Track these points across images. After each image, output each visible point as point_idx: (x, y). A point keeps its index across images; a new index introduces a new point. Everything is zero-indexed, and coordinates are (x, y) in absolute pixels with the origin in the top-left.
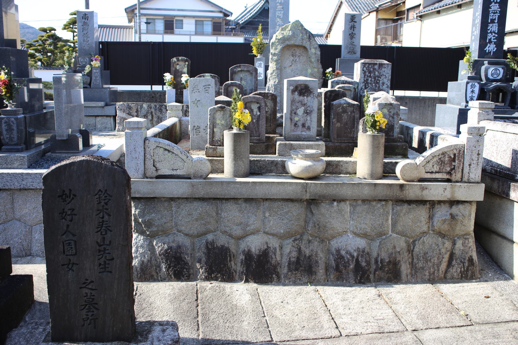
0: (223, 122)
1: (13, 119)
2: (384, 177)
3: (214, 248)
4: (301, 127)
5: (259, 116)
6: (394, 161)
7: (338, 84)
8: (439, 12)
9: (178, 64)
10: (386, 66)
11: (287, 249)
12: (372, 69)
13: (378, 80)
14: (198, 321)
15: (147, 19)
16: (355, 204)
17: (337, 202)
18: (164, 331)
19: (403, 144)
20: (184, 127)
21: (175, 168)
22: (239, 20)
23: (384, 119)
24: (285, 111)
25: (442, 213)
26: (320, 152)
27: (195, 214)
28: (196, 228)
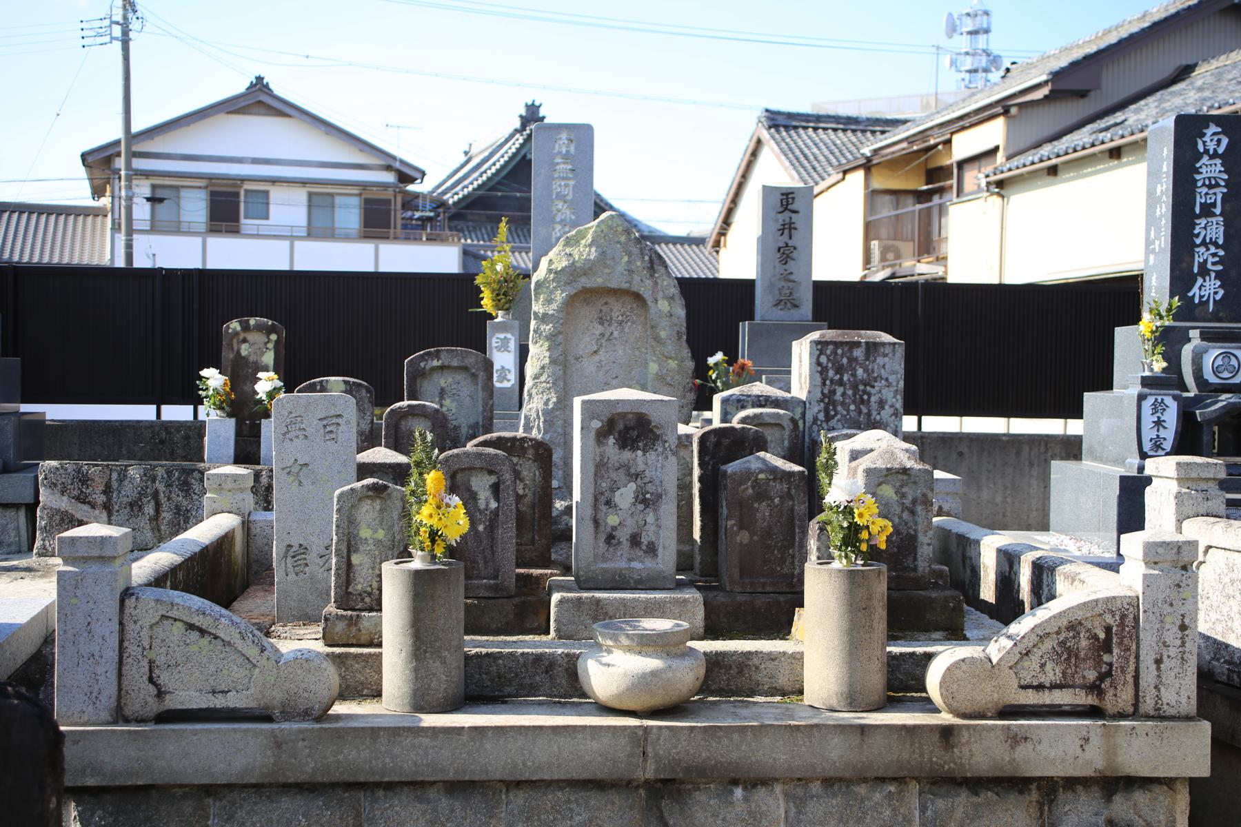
0: (381, 534)
2: (889, 703)
4: (626, 545)
5: (496, 513)
6: (920, 650)
7: (743, 407)
8: (1053, 171)
9: (245, 341)
10: (888, 350)
12: (845, 361)
13: (865, 392)
15: (154, 187)
16: (800, 792)
17: (745, 789)
19: (948, 593)
20: (259, 541)
21: (223, 687)
22: (444, 193)
23: (882, 522)
24: (577, 496)
26: (686, 625)
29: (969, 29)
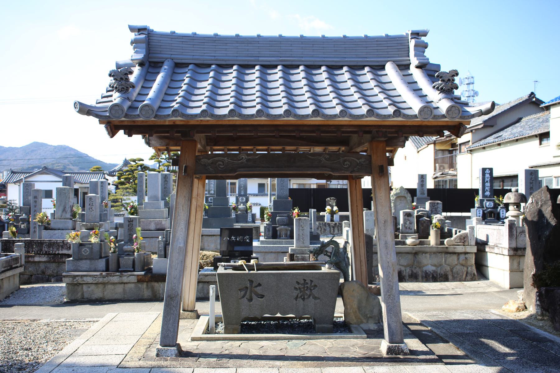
8: (484, 148)
11: (408, 271)
25: (462, 257)
29: (467, 83)
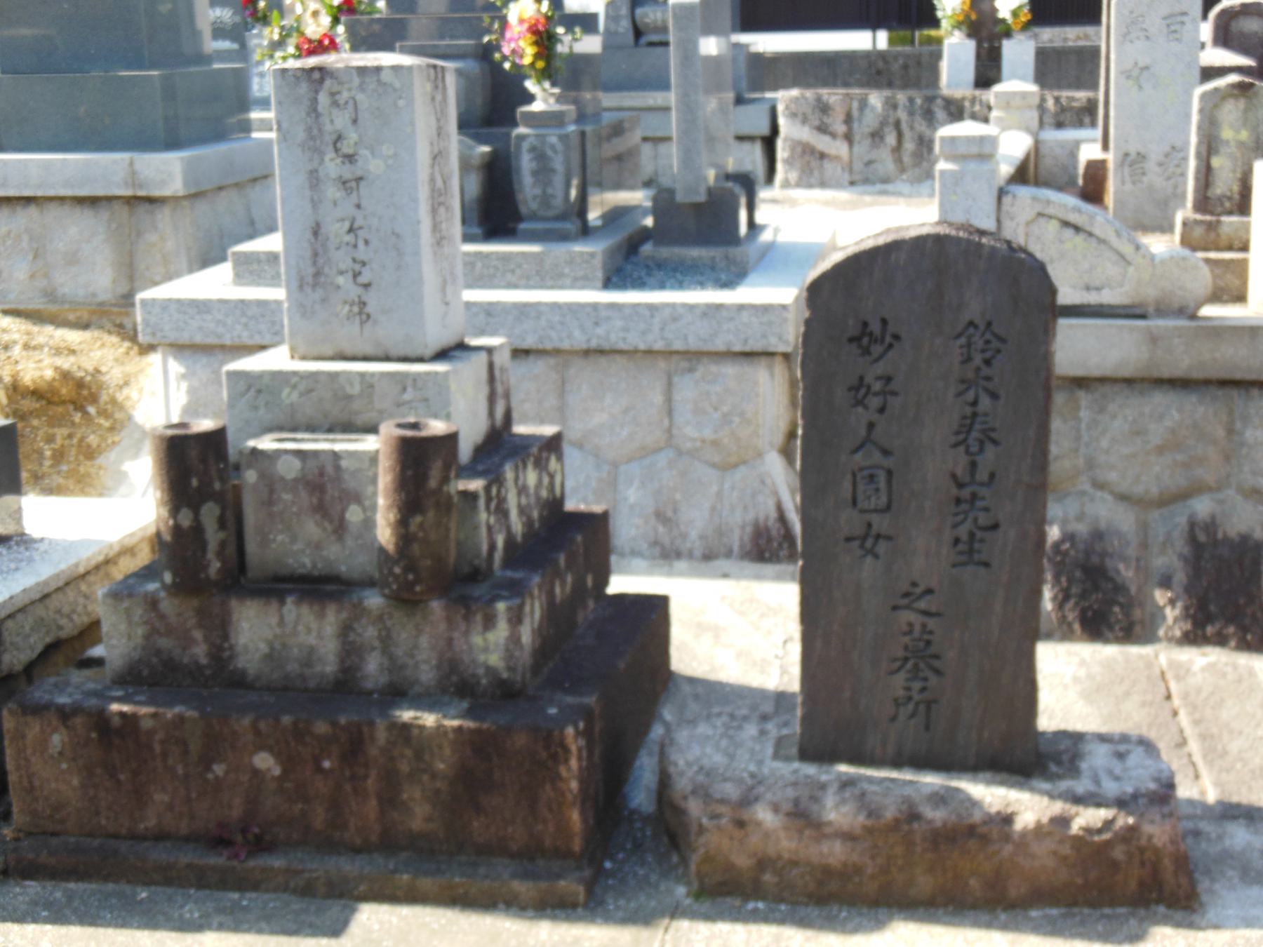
1: (554, 140)
3: (1215, 543)
14: (1190, 755)
18: (1121, 756)
21: (1097, 283)
27: (1157, 433)
28: (1155, 476)
